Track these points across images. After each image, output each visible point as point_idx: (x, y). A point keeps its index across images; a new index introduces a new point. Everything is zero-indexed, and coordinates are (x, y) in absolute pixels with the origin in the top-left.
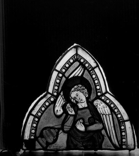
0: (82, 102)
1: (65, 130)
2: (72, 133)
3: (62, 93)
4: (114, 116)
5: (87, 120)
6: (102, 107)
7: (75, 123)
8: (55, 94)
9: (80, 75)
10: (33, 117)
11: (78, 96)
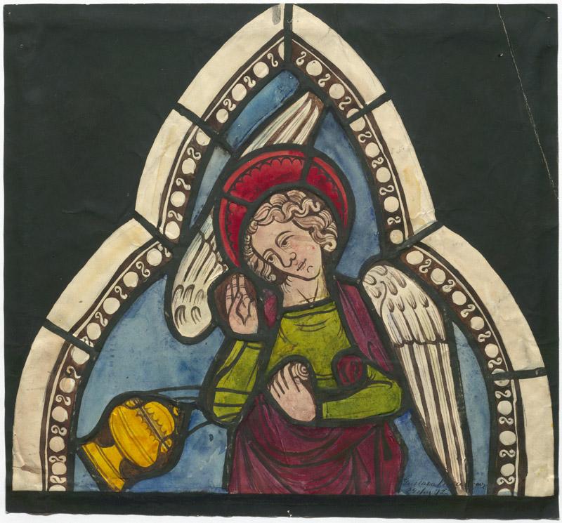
0: (302, 273)
1: (218, 412)
2: (257, 427)
3: (208, 228)
4: (465, 354)
5: (323, 367)
6: (400, 303)
7: (265, 374)
8: (173, 232)
9: (301, 140)
10: (59, 341)
11: (284, 243)
